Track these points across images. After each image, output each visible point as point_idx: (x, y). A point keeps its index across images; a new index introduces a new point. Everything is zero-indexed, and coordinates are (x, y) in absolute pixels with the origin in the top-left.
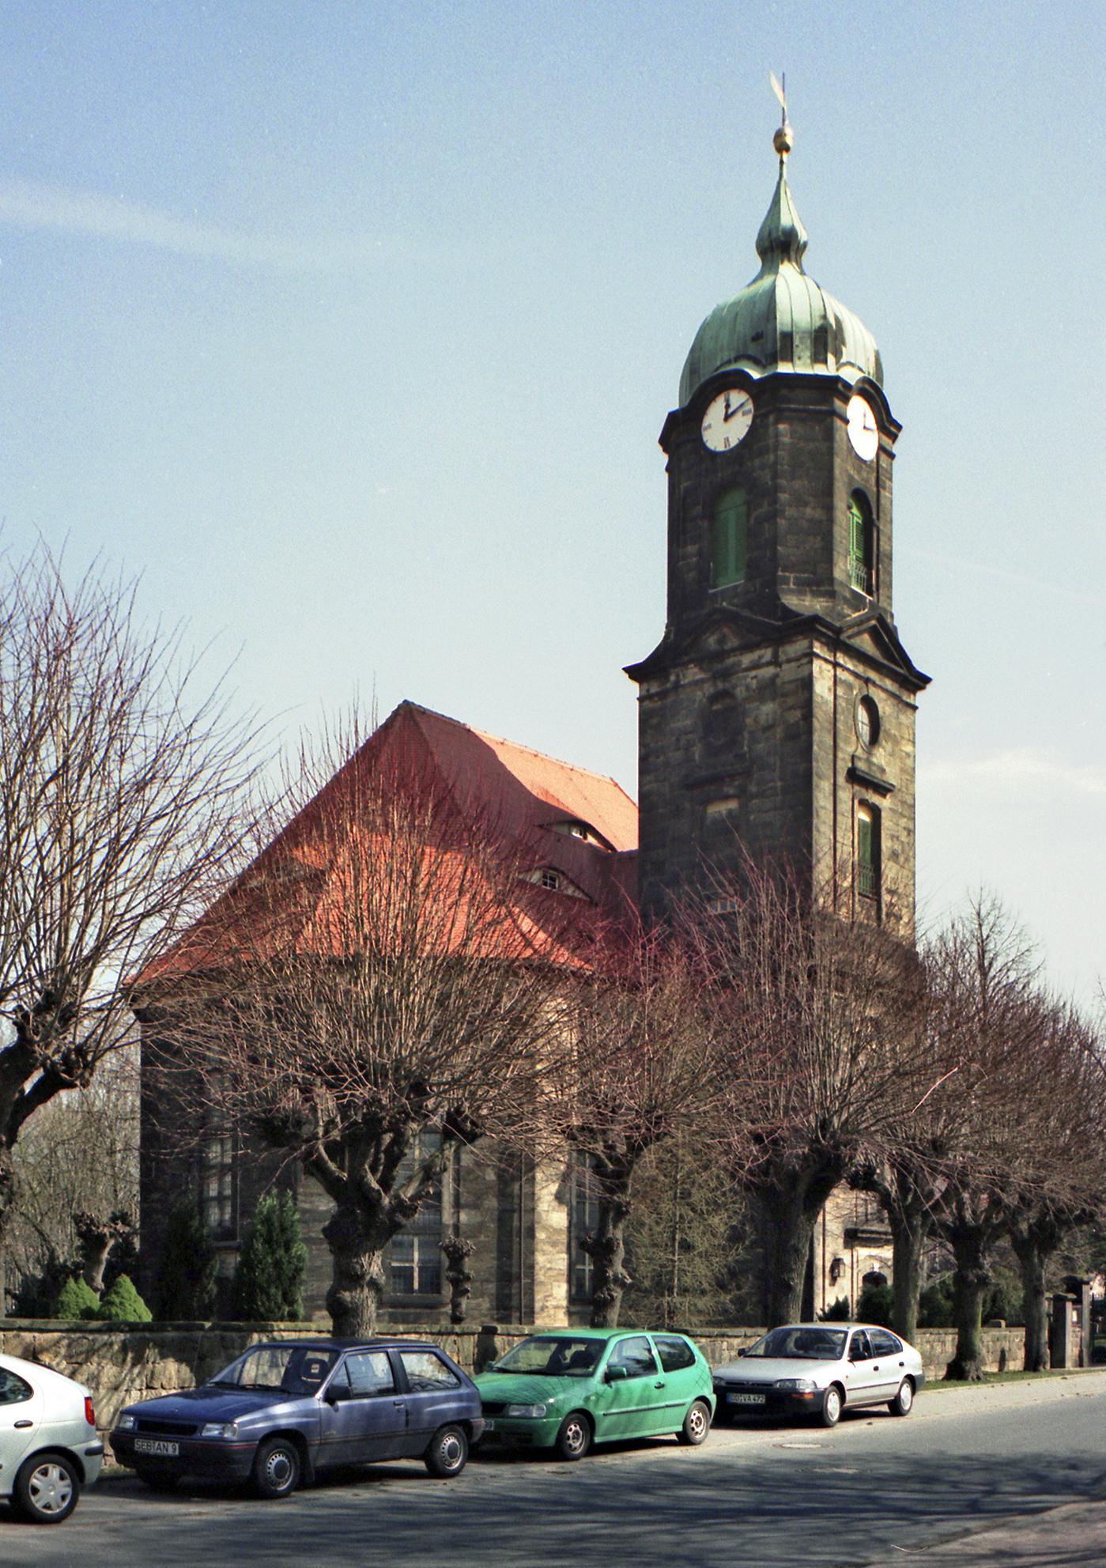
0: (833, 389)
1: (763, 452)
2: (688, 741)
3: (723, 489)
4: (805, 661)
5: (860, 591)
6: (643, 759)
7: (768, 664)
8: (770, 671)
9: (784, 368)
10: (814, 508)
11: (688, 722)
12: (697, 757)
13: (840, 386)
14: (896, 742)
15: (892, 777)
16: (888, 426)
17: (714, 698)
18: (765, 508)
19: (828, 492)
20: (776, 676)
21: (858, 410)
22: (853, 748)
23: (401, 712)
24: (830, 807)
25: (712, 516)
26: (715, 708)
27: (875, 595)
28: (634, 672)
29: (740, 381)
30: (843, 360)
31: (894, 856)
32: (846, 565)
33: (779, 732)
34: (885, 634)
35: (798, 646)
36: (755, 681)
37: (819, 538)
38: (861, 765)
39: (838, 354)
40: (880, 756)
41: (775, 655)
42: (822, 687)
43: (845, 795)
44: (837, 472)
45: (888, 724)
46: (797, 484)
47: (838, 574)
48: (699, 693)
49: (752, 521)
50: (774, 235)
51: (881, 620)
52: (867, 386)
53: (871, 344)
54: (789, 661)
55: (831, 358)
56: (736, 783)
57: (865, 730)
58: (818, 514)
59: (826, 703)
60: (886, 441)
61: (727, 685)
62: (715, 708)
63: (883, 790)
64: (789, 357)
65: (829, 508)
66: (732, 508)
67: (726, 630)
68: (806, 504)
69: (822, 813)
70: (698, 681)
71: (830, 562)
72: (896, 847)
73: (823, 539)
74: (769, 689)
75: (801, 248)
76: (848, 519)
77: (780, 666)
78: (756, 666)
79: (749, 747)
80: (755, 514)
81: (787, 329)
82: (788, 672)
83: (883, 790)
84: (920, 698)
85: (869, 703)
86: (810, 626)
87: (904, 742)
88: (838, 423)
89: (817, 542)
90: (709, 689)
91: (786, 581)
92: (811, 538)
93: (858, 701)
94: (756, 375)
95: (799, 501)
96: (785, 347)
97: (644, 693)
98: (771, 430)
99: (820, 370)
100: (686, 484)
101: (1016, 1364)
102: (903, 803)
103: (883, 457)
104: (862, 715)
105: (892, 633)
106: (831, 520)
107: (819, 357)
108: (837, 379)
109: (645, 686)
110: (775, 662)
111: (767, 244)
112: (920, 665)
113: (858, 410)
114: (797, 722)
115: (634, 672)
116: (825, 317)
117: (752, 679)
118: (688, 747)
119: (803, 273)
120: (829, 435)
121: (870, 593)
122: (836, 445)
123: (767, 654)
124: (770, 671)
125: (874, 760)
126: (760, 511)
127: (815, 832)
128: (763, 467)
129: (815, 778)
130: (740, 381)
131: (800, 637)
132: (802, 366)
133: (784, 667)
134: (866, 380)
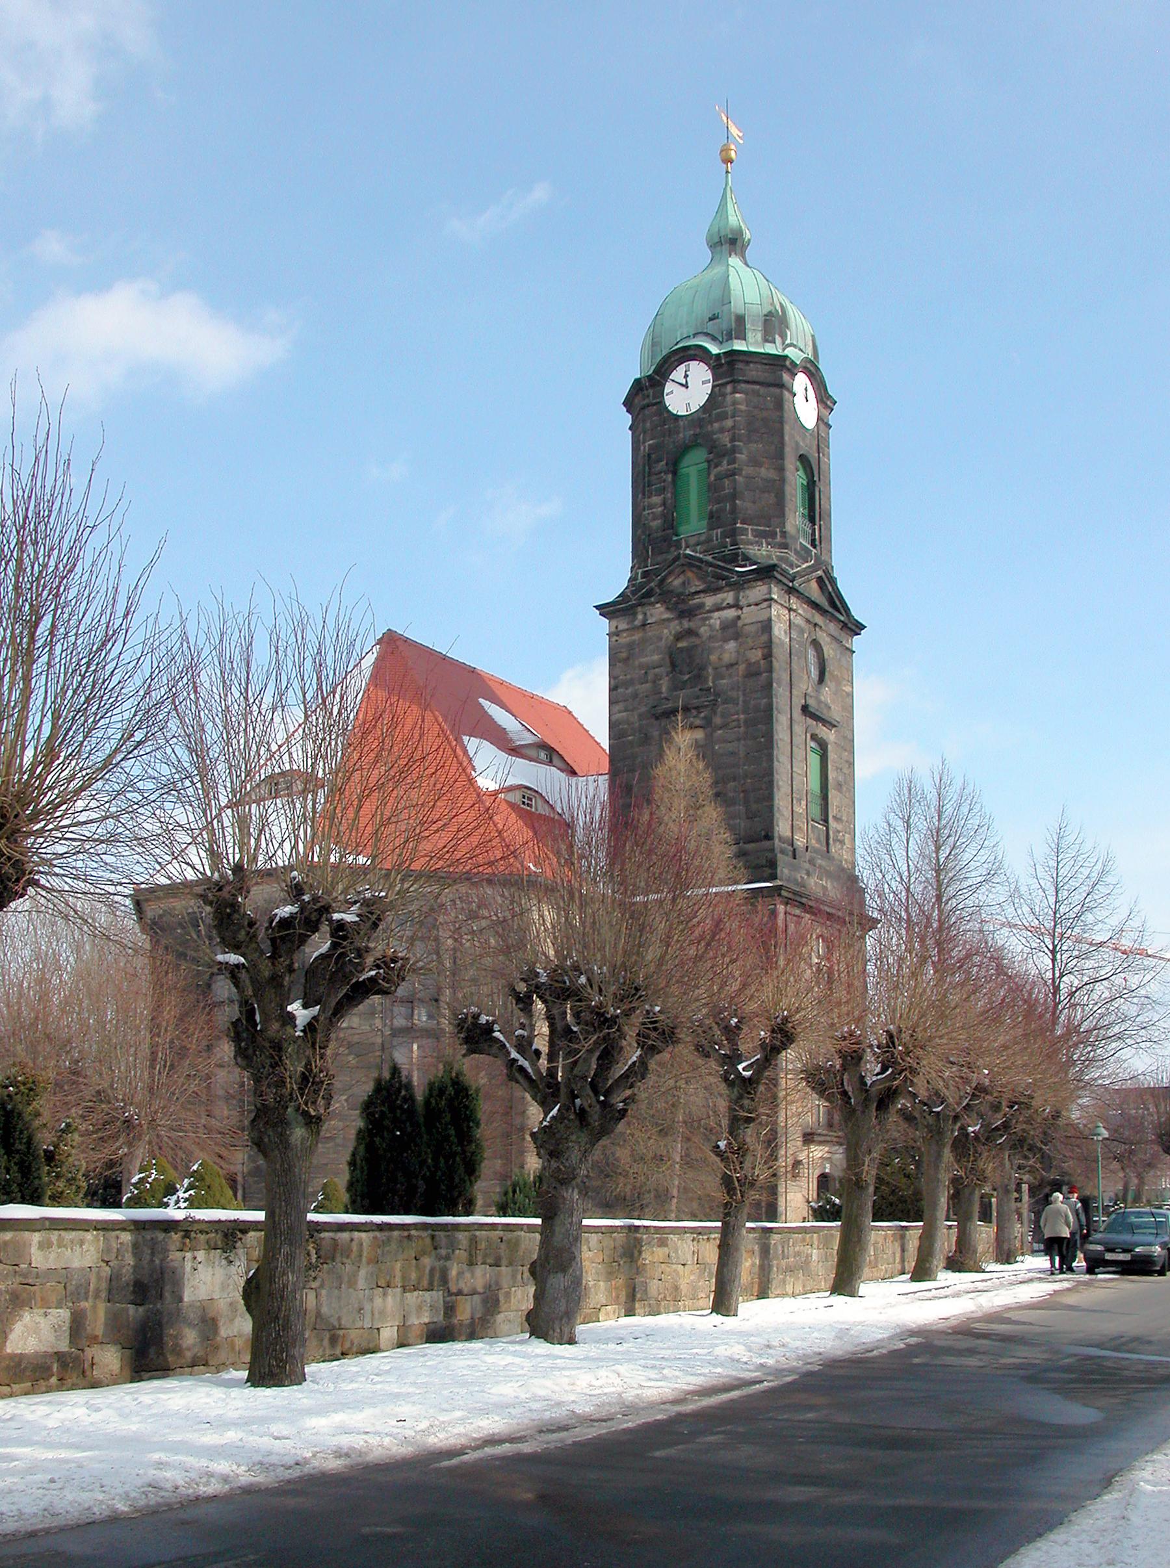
0: (779, 363)
1: (723, 417)
2: (656, 675)
3: (686, 449)
4: (765, 604)
5: (806, 544)
6: (612, 689)
7: (729, 606)
8: (731, 613)
9: (739, 346)
10: (768, 469)
11: (656, 657)
12: (664, 689)
13: (788, 363)
14: (838, 684)
15: (835, 714)
16: (825, 400)
17: (679, 637)
18: (725, 466)
19: (780, 455)
20: (739, 618)
21: (801, 382)
22: (805, 687)
23: (385, 639)
24: (787, 739)
25: (674, 468)
26: (680, 645)
27: (818, 548)
28: (604, 610)
29: (700, 354)
30: (788, 341)
31: (839, 786)
32: (795, 520)
33: (742, 667)
34: (827, 582)
35: (758, 591)
36: (718, 622)
37: (773, 495)
38: (812, 702)
39: (783, 337)
40: (827, 693)
41: (737, 599)
42: (779, 630)
43: (798, 729)
44: (786, 438)
45: (830, 667)
46: (753, 446)
47: (789, 528)
48: (666, 631)
49: (712, 478)
50: (722, 234)
51: (826, 572)
52: (809, 366)
53: (809, 330)
54: (749, 606)
55: (778, 339)
56: (702, 715)
57: (814, 673)
58: (772, 475)
59: (783, 643)
60: (825, 412)
61: (692, 625)
62: (680, 645)
63: (830, 724)
64: (742, 337)
65: (781, 469)
66: (693, 465)
67: (690, 574)
68: (760, 465)
69: (780, 744)
70: (664, 620)
71: (782, 515)
72: (840, 778)
73: (776, 496)
74: (732, 630)
75: (744, 247)
76: (796, 479)
77: (741, 609)
78: (719, 608)
79: (713, 682)
80: (714, 472)
81: (741, 311)
82: (750, 615)
83: (830, 724)
84: (857, 642)
85: (816, 644)
86: (766, 573)
87: (845, 682)
88: (786, 393)
89: (771, 499)
90: (675, 627)
91: (744, 532)
92: (766, 495)
93: (808, 644)
94: (714, 350)
95: (755, 462)
96: (738, 328)
97: (613, 629)
98: (729, 398)
99: (770, 349)
100: (651, 442)
101: (425, 1283)
102: (845, 737)
103: (822, 426)
104: (811, 654)
105: (833, 581)
106: (783, 480)
107: (768, 338)
108: (786, 357)
109: (614, 623)
110: (737, 606)
111: (717, 240)
112: (857, 614)
113: (801, 382)
114: (758, 662)
115: (604, 610)
116: (772, 304)
117: (716, 619)
118: (657, 678)
119: (746, 264)
120: (779, 404)
121: (814, 547)
122: (785, 415)
123: (729, 597)
124: (731, 613)
125: (823, 698)
126: (719, 468)
127: (776, 763)
128: (722, 430)
129: (775, 712)
130: (700, 354)
131: (760, 583)
132: (752, 343)
133: (745, 610)
134: (807, 360)
